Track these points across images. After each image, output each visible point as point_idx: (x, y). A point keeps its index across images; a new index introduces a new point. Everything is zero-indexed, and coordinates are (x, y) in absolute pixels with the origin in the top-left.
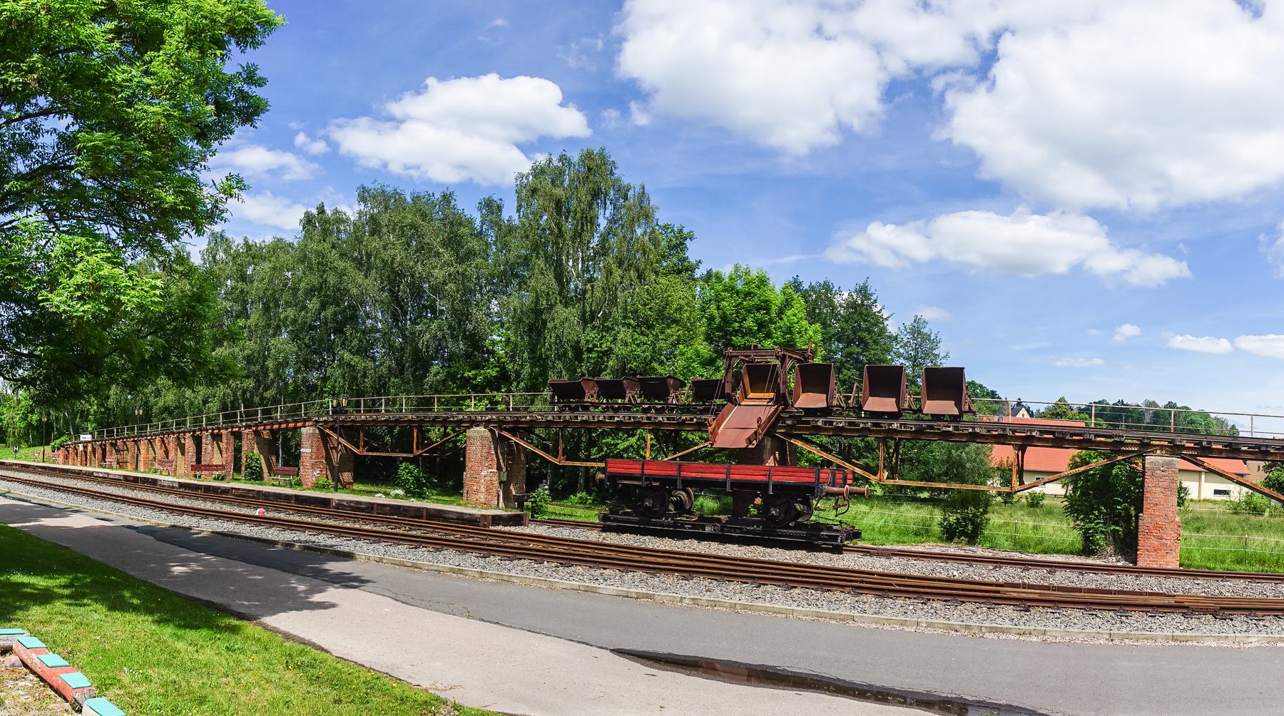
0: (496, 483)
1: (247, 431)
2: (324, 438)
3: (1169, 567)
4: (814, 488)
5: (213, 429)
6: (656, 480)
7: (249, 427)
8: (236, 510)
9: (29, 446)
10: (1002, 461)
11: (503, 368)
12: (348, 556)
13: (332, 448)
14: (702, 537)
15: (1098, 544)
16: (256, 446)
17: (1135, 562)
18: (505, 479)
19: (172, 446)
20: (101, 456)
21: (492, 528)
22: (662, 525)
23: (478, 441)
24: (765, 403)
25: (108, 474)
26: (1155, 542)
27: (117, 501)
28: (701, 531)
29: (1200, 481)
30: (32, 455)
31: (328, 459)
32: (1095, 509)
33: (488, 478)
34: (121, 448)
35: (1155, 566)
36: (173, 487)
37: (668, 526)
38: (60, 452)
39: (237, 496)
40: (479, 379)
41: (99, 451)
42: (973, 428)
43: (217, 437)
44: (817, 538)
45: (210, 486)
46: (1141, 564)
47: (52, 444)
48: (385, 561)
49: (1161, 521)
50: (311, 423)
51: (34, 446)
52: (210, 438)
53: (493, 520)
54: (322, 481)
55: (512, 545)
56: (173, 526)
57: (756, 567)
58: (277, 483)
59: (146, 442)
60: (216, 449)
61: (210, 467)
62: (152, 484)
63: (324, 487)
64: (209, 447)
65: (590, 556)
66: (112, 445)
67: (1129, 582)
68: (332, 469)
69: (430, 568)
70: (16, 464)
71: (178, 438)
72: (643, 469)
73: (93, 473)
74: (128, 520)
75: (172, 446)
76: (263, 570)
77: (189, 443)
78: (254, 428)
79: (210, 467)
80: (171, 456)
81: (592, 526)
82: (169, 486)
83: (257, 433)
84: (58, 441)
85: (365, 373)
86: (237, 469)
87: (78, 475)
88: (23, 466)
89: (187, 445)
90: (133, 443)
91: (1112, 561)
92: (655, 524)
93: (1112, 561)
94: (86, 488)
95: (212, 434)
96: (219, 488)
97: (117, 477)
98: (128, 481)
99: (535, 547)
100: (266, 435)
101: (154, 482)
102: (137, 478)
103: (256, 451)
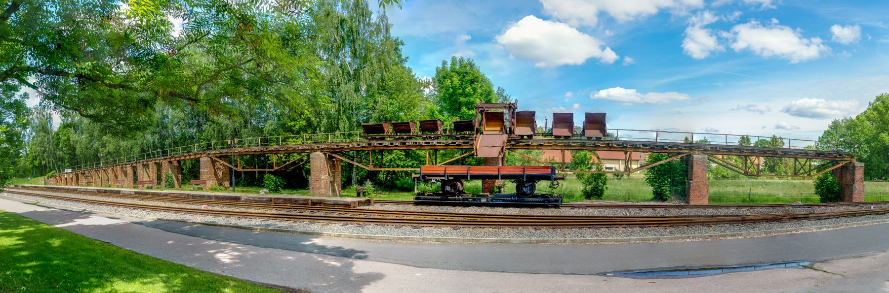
0: (329, 182)
1: (164, 161)
2: (213, 162)
3: (705, 204)
4: (550, 177)
5: (143, 162)
6: (450, 176)
7: (166, 159)
8: (189, 206)
9: (34, 177)
10: (546, 159)
11: (308, 120)
12: (318, 235)
13: (217, 169)
14: (480, 205)
15: (667, 196)
16: (170, 169)
17: (688, 202)
18: (332, 180)
19: (119, 173)
20: (76, 180)
21: (358, 208)
22: (456, 200)
23: (318, 161)
24: (498, 133)
25: (87, 189)
26: (698, 194)
27: (108, 205)
28: (478, 202)
29: (619, 163)
30: (40, 182)
31: (216, 174)
32: (665, 180)
33: (325, 180)
34: (87, 175)
35: (698, 204)
36: (131, 194)
37: (459, 200)
38: (52, 179)
39: (173, 197)
40: (297, 127)
41: (75, 178)
42: (612, 144)
43: (146, 166)
44: (548, 201)
45: (155, 193)
46: (692, 203)
47: (48, 175)
48: (342, 236)
49: (701, 184)
50: (205, 155)
51: (37, 177)
52: (141, 166)
53: (358, 203)
54: (214, 186)
55: (389, 218)
56: (158, 219)
57: (555, 219)
58: (191, 189)
59: (102, 171)
60: (145, 172)
61: (143, 183)
62: (117, 193)
63: (215, 190)
64: (141, 171)
65: (425, 220)
66: (82, 174)
67: (685, 212)
68: (218, 179)
69: (382, 238)
70: (31, 187)
71: (122, 168)
72: (445, 171)
73: (77, 189)
74: (130, 218)
75: (119, 173)
76: (292, 253)
77: (129, 170)
78: (169, 160)
79: (143, 183)
80: (119, 177)
81: (409, 203)
82: (128, 194)
83: (170, 162)
84: (50, 174)
85: (227, 127)
86: (159, 183)
87: (68, 190)
88: (35, 187)
89: (128, 171)
90: (95, 172)
91: (677, 203)
92: (450, 200)
93: (677, 203)
94: (77, 197)
95: (143, 165)
96: (161, 193)
97: (93, 191)
98: (100, 192)
99: (408, 218)
100: (176, 164)
101: (119, 192)
102: (106, 190)
103: (170, 172)
